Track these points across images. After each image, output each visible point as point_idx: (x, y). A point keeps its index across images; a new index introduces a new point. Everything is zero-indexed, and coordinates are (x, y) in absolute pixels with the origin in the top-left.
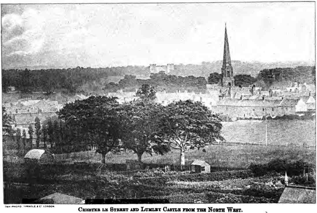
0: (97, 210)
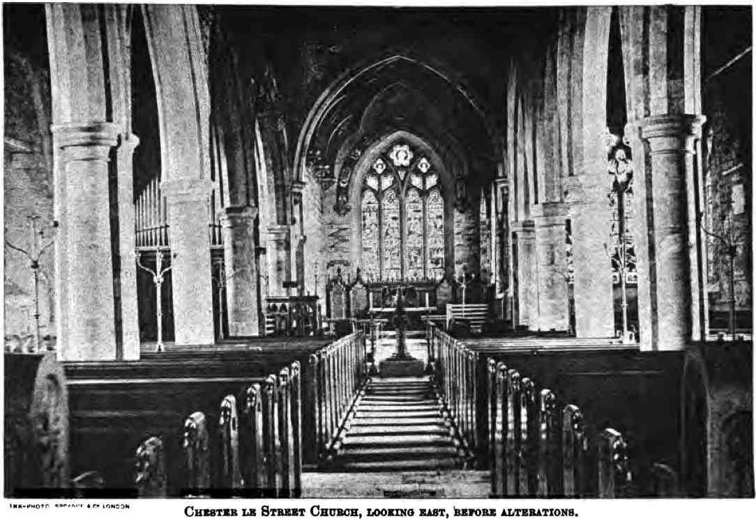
0: (529, 512)
